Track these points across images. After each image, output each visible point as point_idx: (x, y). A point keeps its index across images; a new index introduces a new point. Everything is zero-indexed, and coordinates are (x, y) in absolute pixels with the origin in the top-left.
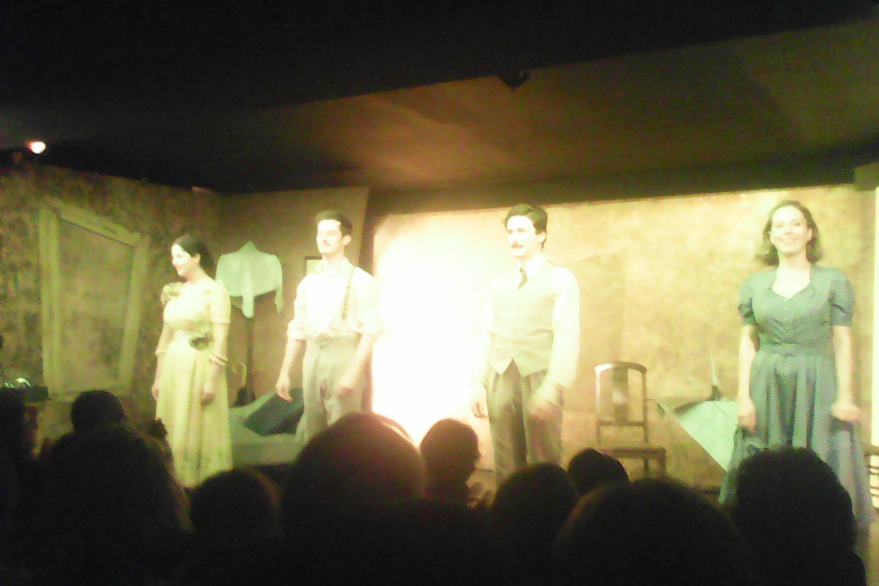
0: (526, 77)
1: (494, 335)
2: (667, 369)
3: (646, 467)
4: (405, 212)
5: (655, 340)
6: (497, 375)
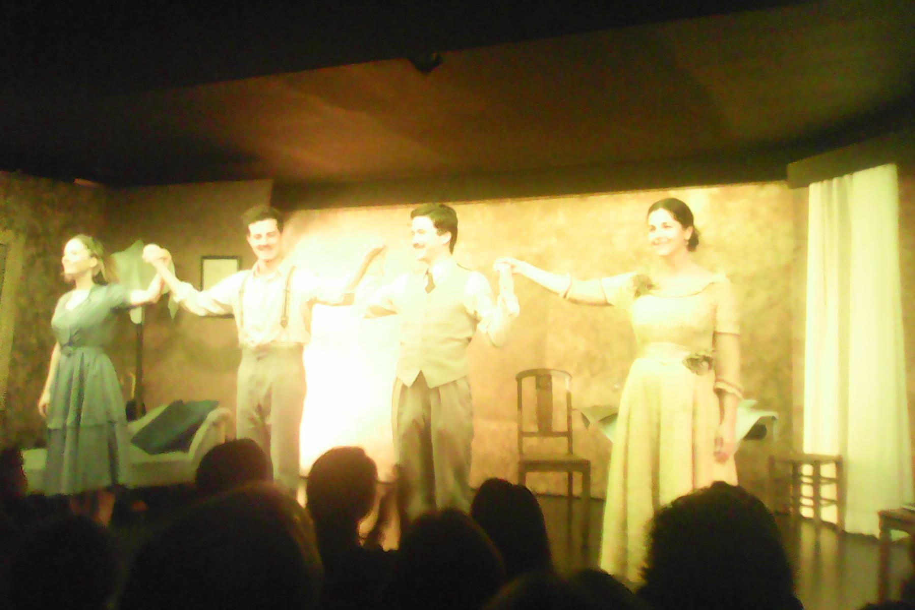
0: (438, 62)
1: (402, 343)
2: (593, 375)
3: (808, 484)
4: (314, 207)
5: (582, 345)
6: (404, 387)
